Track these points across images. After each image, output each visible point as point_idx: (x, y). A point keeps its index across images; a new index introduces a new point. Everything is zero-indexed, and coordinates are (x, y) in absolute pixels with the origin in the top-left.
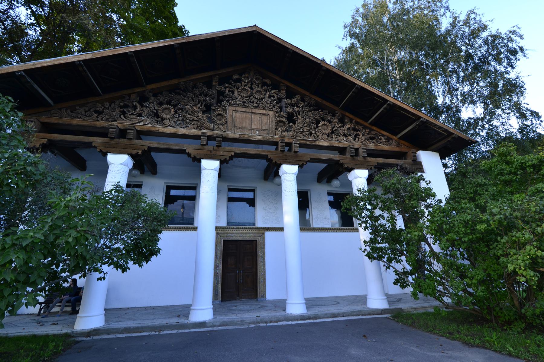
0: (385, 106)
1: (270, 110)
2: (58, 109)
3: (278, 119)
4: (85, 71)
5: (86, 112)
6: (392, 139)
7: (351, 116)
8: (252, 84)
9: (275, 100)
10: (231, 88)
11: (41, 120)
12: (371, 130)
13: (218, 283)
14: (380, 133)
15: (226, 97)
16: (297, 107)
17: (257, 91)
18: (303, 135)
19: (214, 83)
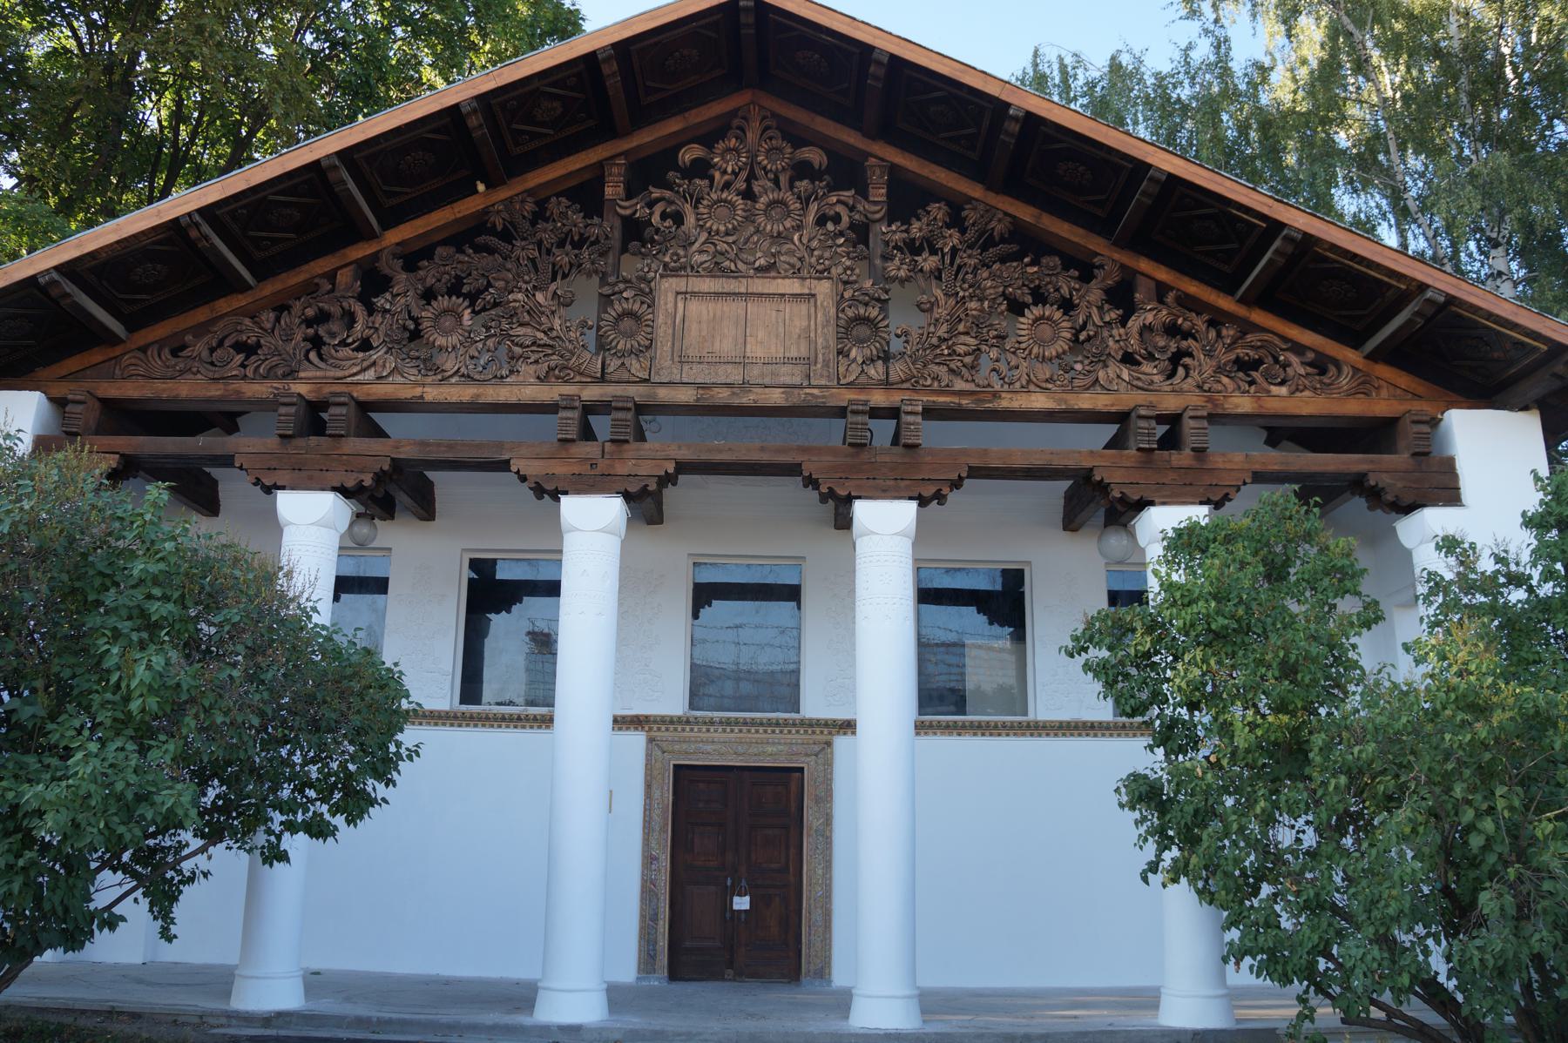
0: (1277, 244)
1: (822, 274)
2: (139, 349)
3: (850, 313)
4: (206, 238)
5: (212, 350)
6: (1337, 364)
7: (1163, 274)
8: (751, 177)
9: (841, 234)
10: (671, 203)
11: (101, 393)
12: (1247, 327)
13: (655, 918)
14: (1284, 339)
15: (653, 241)
16: (933, 252)
17: (772, 204)
18: (951, 371)
19: (609, 191)
